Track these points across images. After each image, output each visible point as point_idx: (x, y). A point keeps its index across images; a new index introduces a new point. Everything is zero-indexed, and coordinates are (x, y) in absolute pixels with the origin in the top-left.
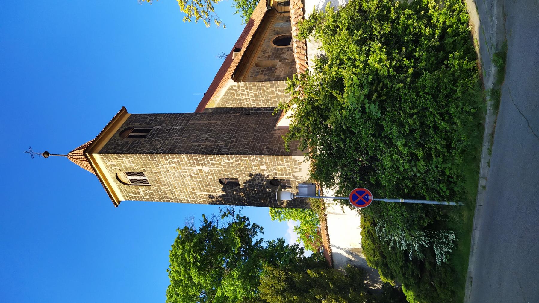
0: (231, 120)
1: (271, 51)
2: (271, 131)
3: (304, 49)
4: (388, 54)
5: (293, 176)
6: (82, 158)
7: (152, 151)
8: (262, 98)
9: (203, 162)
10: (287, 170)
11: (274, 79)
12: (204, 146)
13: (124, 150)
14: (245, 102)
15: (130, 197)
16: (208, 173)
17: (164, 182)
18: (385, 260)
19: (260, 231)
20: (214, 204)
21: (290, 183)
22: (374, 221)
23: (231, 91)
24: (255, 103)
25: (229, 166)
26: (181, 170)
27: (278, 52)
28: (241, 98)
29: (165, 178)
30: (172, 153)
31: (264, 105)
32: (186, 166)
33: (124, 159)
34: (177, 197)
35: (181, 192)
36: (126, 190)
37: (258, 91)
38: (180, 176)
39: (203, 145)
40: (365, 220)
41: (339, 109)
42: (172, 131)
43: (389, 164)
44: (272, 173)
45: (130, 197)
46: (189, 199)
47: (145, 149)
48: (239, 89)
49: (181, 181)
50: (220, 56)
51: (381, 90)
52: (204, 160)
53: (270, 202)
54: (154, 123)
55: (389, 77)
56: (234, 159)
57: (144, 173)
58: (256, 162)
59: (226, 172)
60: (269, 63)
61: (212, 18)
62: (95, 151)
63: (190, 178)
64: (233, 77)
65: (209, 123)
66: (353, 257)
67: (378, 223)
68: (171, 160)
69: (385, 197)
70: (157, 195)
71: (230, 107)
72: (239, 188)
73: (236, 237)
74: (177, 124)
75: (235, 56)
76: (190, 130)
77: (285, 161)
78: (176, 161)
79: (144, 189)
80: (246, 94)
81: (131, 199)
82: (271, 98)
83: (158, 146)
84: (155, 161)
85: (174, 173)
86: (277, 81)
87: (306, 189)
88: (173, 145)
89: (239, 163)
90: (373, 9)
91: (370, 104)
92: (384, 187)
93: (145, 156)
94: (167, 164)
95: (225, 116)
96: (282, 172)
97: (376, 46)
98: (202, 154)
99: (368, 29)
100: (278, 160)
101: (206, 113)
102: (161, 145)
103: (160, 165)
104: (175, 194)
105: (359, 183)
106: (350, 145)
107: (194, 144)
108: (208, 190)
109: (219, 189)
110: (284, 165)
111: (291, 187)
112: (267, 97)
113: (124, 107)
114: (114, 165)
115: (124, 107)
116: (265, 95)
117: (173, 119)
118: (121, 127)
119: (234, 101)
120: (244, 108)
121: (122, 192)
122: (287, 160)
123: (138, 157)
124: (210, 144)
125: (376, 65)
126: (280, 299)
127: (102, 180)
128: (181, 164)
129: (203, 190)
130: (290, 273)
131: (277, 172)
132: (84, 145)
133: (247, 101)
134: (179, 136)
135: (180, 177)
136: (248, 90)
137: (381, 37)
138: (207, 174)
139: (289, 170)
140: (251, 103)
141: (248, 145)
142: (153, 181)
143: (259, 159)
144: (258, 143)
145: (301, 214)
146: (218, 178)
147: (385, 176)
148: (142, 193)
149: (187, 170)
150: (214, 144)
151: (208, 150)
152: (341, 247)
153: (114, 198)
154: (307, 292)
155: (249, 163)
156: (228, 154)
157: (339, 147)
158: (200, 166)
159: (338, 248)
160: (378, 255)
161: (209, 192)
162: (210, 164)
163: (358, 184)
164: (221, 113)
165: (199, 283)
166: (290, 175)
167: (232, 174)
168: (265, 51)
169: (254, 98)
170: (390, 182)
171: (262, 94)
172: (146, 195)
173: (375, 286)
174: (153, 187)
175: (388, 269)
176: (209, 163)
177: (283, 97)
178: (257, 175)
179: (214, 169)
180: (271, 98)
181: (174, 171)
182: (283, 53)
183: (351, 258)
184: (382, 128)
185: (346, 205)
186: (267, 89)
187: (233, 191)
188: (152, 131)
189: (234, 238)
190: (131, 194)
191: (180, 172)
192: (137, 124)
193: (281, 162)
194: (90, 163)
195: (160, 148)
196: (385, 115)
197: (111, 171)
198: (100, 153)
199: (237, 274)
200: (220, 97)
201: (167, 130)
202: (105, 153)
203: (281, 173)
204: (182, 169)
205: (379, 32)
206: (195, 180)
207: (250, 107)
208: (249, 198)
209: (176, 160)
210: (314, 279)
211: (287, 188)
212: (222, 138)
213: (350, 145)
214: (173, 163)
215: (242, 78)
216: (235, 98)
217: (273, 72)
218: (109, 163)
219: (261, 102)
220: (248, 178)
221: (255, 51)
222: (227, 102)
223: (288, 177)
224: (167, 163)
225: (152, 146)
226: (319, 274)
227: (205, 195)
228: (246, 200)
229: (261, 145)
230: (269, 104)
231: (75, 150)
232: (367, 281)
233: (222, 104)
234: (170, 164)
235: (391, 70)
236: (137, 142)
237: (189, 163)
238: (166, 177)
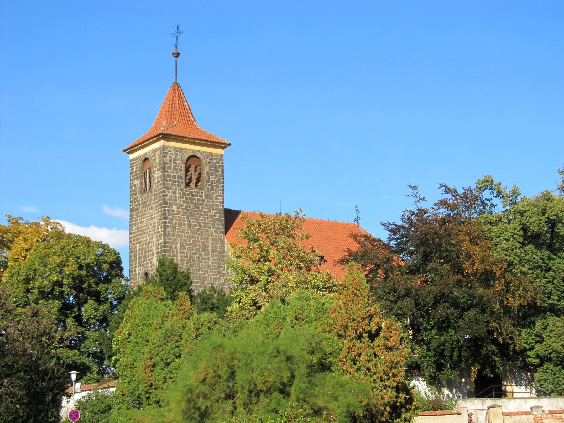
0: (213, 275)
12: (176, 258)
39: (177, 256)
65: (208, 252)
76: (199, 234)
107: (178, 245)
149: (153, 240)
225: (176, 200)
234: (158, 223)
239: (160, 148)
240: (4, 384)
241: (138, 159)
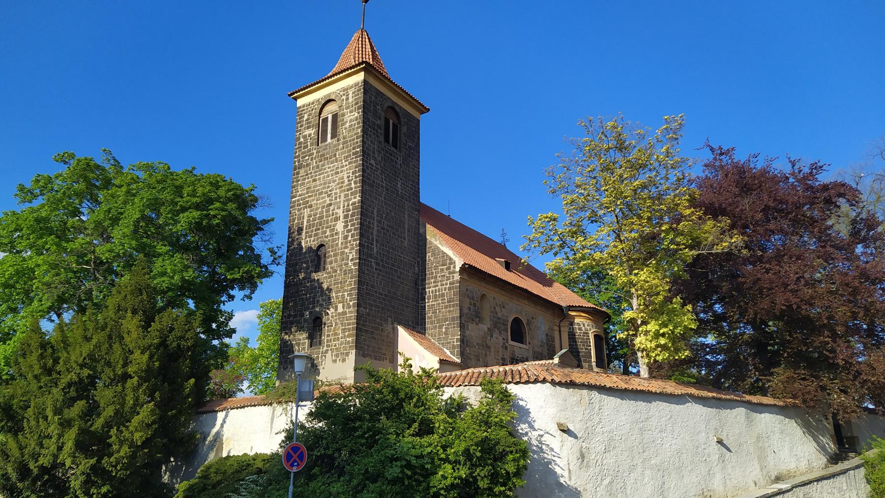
0: (409, 260)
1: (503, 315)
2: (391, 318)
3: (475, 383)
4: (453, 486)
5: (327, 351)
6: (359, 51)
7: (366, 154)
9: (350, 224)
11: (463, 322)
13: (367, 114)
14: (432, 280)
15: (301, 114)
17: (322, 166)
18: (210, 487)
19: (245, 296)
20: (289, 234)
21: (316, 345)
22: (265, 473)
23: (448, 261)
24: (431, 294)
27: (501, 325)
28: (439, 275)
29: (329, 168)
30: (363, 182)
31: (428, 306)
33: (356, 114)
34: (300, 182)
35: (307, 189)
36: (312, 110)
39: (373, 224)
40: (264, 460)
41: (398, 431)
42: (395, 179)
43: (334, 490)
45: (301, 114)
46: (298, 198)
47: (369, 143)
48: (450, 273)
49: (324, 191)
50: (504, 235)
51: (415, 479)
52: (353, 225)
53: (289, 316)
54: (405, 152)
55: (428, 488)
56: (352, 267)
57: (336, 139)
58: (348, 298)
59: (335, 255)
60: (486, 314)
61: (530, 253)
62: (367, 75)
64: (467, 266)
65: (405, 229)
66: (210, 442)
67: (262, 478)
68: (352, 179)
69: (295, 486)
70: (303, 153)
71: (427, 259)
72: (312, 272)
73: (241, 271)
74: (404, 185)
75: (499, 262)
77: (348, 339)
79: (313, 135)
81: (299, 115)
82: (438, 317)
83: (373, 162)
85: (336, 181)
86: (460, 327)
87: (307, 390)
88: (374, 181)
90: (506, 466)
91: (400, 467)
92: (307, 484)
93: (359, 144)
94: (347, 173)
95: (414, 251)
96: (332, 334)
97: (463, 472)
98: (361, 224)
99: (481, 462)
100: (349, 330)
101: (419, 225)
102: (374, 164)
103: (347, 163)
105: (313, 455)
106: (358, 443)
107: (375, 211)
108: (309, 227)
109: (310, 242)
110: (342, 338)
111: (311, 347)
112: (439, 312)
113: (429, 110)
114: (347, 99)
115: (429, 110)
116: (442, 309)
117: (411, 178)
118: (401, 108)
120: (425, 278)
122: (349, 343)
123: (358, 133)
124: (375, 233)
125: (441, 473)
126: (154, 341)
127: (327, 81)
128: (347, 193)
129: (310, 219)
130: (190, 353)
131: (332, 328)
132: (377, 53)
134: (387, 189)
135: (329, 189)
136: (448, 286)
137: (473, 477)
139: (335, 346)
140: (432, 289)
141: (373, 286)
142: (324, 150)
143: (351, 303)
144: (375, 301)
145: (269, 349)
147: (320, 486)
148: (307, 132)
149: (338, 200)
150: (375, 240)
151: (366, 231)
152: (225, 425)
153: (301, 92)
154: (163, 381)
155: (346, 288)
156: (360, 259)
157: (355, 429)
158: (344, 218)
159: (224, 421)
160: (217, 479)
161: (306, 229)
162: (346, 234)
163: (312, 453)
164: (418, 246)
165: (176, 222)
166: (328, 346)
167: (331, 263)
168: (504, 307)
169: (437, 293)
170: (312, 491)
172: (305, 137)
173: (165, 473)
174: (315, 149)
175: (200, 492)
176: (349, 231)
177: (439, 335)
178: (330, 299)
180: (438, 317)
182: (500, 333)
183: (209, 439)
184: (375, 481)
185: (285, 437)
186: (450, 311)
187: (306, 263)
188: (395, 150)
189: (239, 269)
190: (306, 117)
191: (336, 190)
192: (404, 129)
193: (347, 334)
194: (351, 68)
195: (370, 164)
196: (388, 484)
197: (339, 94)
198: (365, 81)
199: (190, 276)
200: (439, 246)
201: (396, 172)
202: (364, 89)
203: (331, 333)
204: (340, 193)
205: (479, 475)
206: (324, 210)
207: (427, 286)
208: (296, 285)
209: (353, 186)
210: (182, 387)
211: (310, 340)
212: (383, 250)
213: (358, 443)
214: (349, 181)
215: (465, 277)
217: (473, 320)
218: (351, 93)
219: (433, 303)
220: (325, 286)
221: (503, 292)
222: (434, 254)
223: (326, 344)
224: (350, 173)
225: (374, 153)
226: (188, 396)
227: (303, 222)
228: (293, 281)
229: (372, 305)
231: (370, 41)
232: (173, 461)
233: (431, 247)
234: (348, 177)
235: (435, 489)
236: (379, 131)
238: (329, 170)
239: (359, 83)
240: (72, 236)
241: (313, 103)
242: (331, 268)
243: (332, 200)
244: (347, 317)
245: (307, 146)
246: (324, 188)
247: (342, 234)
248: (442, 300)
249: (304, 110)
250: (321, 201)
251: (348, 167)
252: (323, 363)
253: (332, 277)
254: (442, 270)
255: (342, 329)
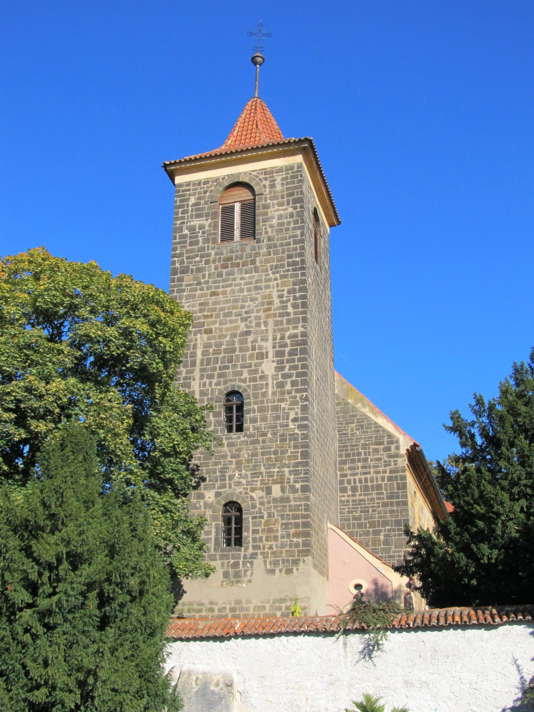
5: (254, 556)
8: (372, 500)
10: (270, 543)
15: (184, 195)
16: (256, 371)
17: (228, 274)
25: (278, 418)
26: (263, 316)
32: (276, 328)
33: (291, 210)
34: (185, 294)
35: (200, 304)
37: (387, 493)
38: (246, 309)
44: (260, 509)
48: (390, 456)
49: (234, 311)
56: (296, 431)
63: (241, 330)
77: (295, 540)
78: (289, 311)
80: (380, 469)
82: (372, 518)
84: (287, 268)
85: (256, 299)
89: (285, 440)
96: (263, 530)
103: (278, 276)
104: (196, 290)
112: (373, 511)
114: (272, 186)
116: (378, 507)
119: (362, 442)
121: (199, 184)
128: (280, 319)
131: (263, 521)
133: (363, 467)
135: (244, 310)
136: (387, 474)
138: (253, 368)
139: (271, 547)
146: (245, 390)
149: (263, 327)
155: (287, 462)
158: (276, 356)
161: (202, 364)
162: (280, 379)
171: (380, 501)
176: (285, 376)
179: (267, 384)
181: (260, 300)
186: (392, 512)
190: (192, 200)
191: (258, 311)
193: (292, 531)
197: (257, 177)
200: (370, 415)
206: (236, 340)
209: (290, 310)
216: (369, 445)
219: (362, 497)
227: (195, 353)
230: (356, 512)
237: (284, 335)
238: (243, 282)
242: (255, 429)
243: (251, 327)
244: (290, 506)
245: (197, 243)
246: (234, 307)
247: (273, 379)
248: (377, 494)
249: (189, 190)
250: (228, 326)
251: (279, 281)
252: (249, 573)
253: (257, 442)
254: (376, 451)
255: (282, 524)
